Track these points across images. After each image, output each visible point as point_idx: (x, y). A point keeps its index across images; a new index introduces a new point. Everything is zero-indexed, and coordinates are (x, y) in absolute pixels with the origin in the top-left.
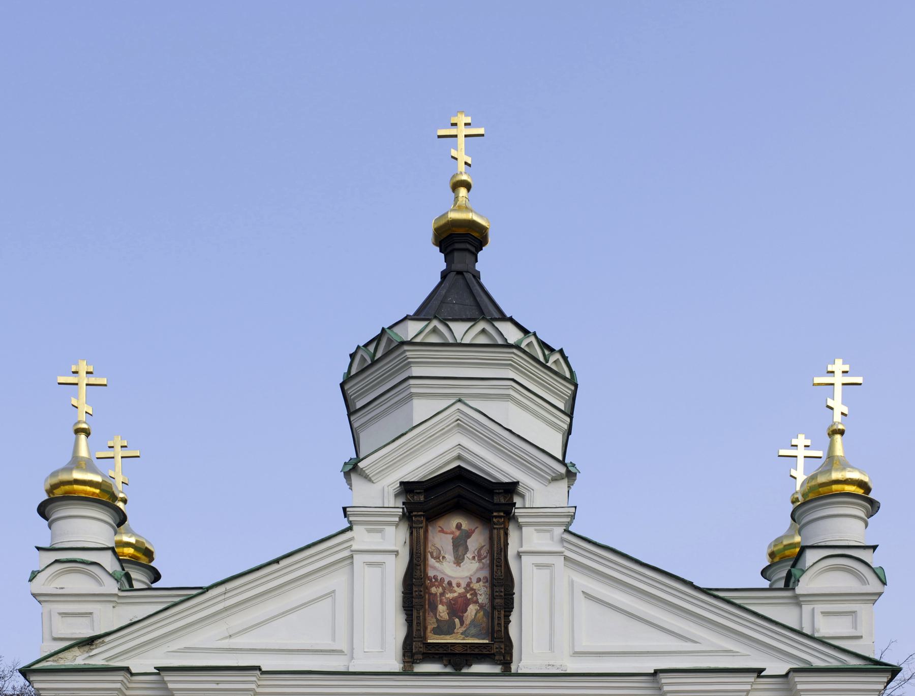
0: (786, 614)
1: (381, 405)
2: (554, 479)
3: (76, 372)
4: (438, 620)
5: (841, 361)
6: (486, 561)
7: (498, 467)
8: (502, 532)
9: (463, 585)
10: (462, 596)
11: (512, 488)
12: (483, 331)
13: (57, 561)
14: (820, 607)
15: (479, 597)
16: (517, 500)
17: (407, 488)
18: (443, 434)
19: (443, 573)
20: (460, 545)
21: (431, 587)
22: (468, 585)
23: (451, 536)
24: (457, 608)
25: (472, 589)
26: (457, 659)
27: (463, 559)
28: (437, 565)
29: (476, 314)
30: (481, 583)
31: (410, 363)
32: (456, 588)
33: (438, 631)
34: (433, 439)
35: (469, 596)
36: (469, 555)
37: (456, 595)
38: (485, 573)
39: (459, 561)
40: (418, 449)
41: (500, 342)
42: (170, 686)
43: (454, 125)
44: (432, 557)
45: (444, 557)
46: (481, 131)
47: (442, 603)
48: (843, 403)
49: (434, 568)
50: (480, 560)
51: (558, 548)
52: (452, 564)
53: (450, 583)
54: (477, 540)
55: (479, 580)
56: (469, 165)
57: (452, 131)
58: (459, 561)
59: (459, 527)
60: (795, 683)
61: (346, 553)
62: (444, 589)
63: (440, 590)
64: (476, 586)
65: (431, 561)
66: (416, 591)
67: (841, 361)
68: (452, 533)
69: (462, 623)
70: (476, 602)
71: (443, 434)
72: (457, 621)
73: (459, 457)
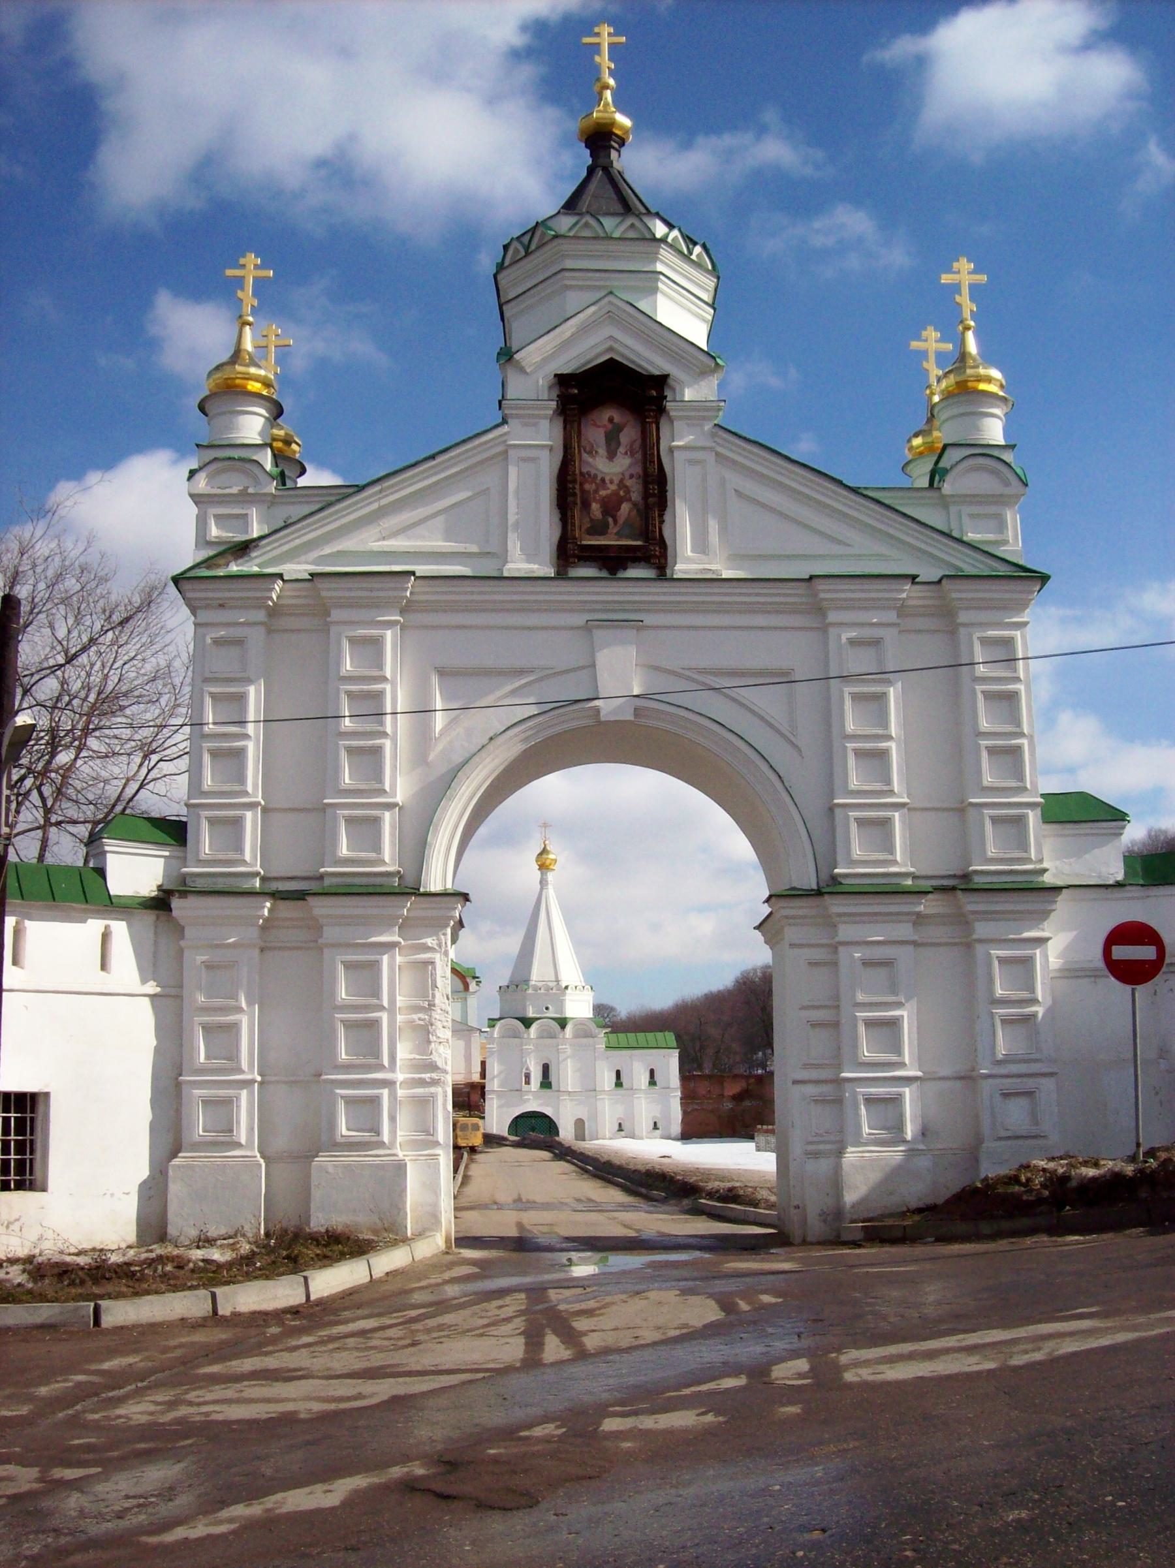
0: (935, 518)
4: (592, 520)
7: (652, 362)
9: (616, 482)
10: (615, 493)
12: (632, 226)
13: (216, 459)
14: (967, 510)
17: (562, 380)
19: (592, 466)
20: (612, 440)
22: (621, 481)
24: (610, 508)
25: (626, 487)
26: (612, 562)
28: (590, 460)
29: (618, 208)
32: (609, 485)
35: (622, 493)
36: (622, 450)
37: (609, 492)
38: (638, 470)
39: (611, 455)
47: (595, 500)
49: (588, 463)
53: (603, 480)
54: (629, 435)
55: (632, 476)
58: (611, 455)
59: (611, 420)
64: (629, 483)
66: (569, 489)
68: (605, 426)
69: (615, 522)
70: (630, 500)
72: (610, 520)
73: (611, 349)
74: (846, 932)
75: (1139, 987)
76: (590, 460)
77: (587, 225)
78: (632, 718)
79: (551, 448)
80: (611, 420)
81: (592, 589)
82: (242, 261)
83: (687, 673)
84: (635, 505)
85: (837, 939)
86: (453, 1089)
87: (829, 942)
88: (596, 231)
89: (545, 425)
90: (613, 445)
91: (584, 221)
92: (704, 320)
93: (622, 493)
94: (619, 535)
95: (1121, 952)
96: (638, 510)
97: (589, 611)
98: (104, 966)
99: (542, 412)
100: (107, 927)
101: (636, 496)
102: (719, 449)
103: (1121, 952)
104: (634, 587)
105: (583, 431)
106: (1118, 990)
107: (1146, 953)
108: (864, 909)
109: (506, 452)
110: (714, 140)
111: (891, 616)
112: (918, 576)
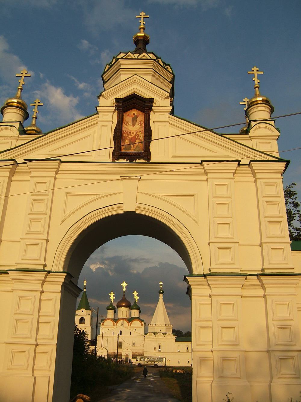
1: (112, 79)
2: (166, 98)
3: (22, 73)
5: (256, 67)
6: (143, 125)
7: (147, 94)
8: (148, 114)
9: (135, 133)
10: (134, 137)
11: (151, 101)
14: (258, 141)
15: (140, 137)
16: (154, 105)
18: (130, 85)
19: (128, 129)
20: (134, 120)
21: (124, 134)
22: (136, 133)
23: (132, 117)
24: (132, 142)
25: (138, 135)
26: (131, 158)
27: (135, 124)
28: (126, 126)
30: (141, 133)
31: (121, 65)
32: (132, 134)
34: (126, 86)
35: (136, 137)
36: (137, 123)
37: (132, 136)
38: (143, 129)
39: (133, 125)
40: (122, 89)
41: (149, 58)
42: (254, 168)
43: (141, 15)
44: (125, 124)
45: (128, 124)
46: (148, 16)
47: (127, 139)
48: (258, 79)
49: (125, 127)
50: (141, 125)
51: (167, 119)
52: (131, 126)
53: (130, 133)
54: (141, 118)
55: (140, 132)
56: (144, 24)
57: (140, 17)
58: (133, 125)
59: (134, 114)
60: (252, 164)
61: (96, 122)
62: (128, 134)
63: (127, 135)
64: (139, 133)
65: (124, 125)
66: (118, 134)
67: (256, 67)
68: (132, 116)
69: (134, 146)
70: (139, 139)
71: (130, 85)
74: (215, 291)
76: (126, 126)
77: (129, 55)
81: (125, 167)
82: (253, 69)
86: (173, 330)
90: (134, 121)
91: (128, 55)
101: (142, 137)
102: (170, 122)
104: (139, 166)
110: (152, 265)
112: (239, 161)
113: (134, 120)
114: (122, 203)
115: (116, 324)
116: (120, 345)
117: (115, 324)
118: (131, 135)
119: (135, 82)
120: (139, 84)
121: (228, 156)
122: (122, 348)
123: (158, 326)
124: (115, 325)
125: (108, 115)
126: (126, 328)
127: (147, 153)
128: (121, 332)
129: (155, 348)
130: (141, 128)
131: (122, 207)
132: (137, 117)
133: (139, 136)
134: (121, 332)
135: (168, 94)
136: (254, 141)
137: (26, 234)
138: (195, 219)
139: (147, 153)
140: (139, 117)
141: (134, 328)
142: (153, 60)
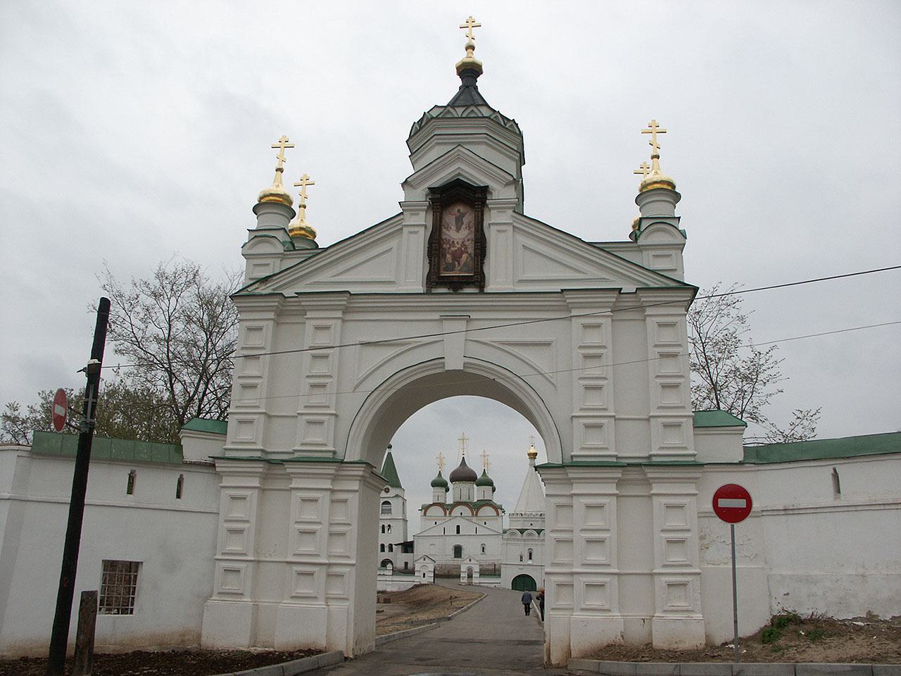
6: (473, 229)
7: (479, 179)
9: (460, 243)
11: (485, 190)
19: (449, 236)
20: (459, 221)
22: (463, 243)
24: (457, 256)
25: (465, 245)
26: (456, 285)
28: (447, 232)
33: (446, 270)
35: (463, 249)
39: (458, 230)
47: (448, 253)
49: (446, 234)
50: (469, 229)
53: (453, 242)
54: (469, 218)
58: (458, 230)
59: (459, 211)
64: (467, 243)
66: (435, 247)
69: (459, 264)
70: (467, 252)
72: (456, 263)
73: (459, 174)
75: (735, 525)
77: (449, 112)
78: (462, 369)
79: (426, 226)
80: (459, 211)
83: (493, 344)
84: (470, 255)
85: (652, 492)
87: (647, 494)
88: (476, 114)
89: (423, 214)
90: (459, 225)
91: (447, 110)
92: (514, 159)
93: (463, 249)
94: (461, 271)
95: (723, 503)
96: (471, 257)
97: (442, 311)
98: (178, 496)
99: (422, 208)
100: (181, 476)
101: (471, 250)
102: (515, 224)
103: (723, 503)
104: (467, 299)
105: (444, 216)
106: (722, 527)
107: (741, 503)
108: (582, 476)
109: (402, 229)
111: (339, 314)
113: (459, 221)
114: (444, 358)
115: (450, 513)
116: (458, 551)
117: (448, 512)
118: (454, 247)
119: (458, 158)
120: (465, 161)
121: (605, 279)
122: (461, 557)
123: (526, 518)
124: (448, 515)
125: (418, 214)
126: (467, 520)
127: (479, 277)
128: (458, 527)
129: (521, 557)
130: (470, 234)
131: (444, 363)
132: (464, 216)
133: (467, 248)
134: (458, 527)
135: (511, 179)
136: (645, 253)
137: (305, 407)
138: (552, 380)
139: (479, 277)
140: (466, 216)
141: (483, 520)
142: (487, 119)
